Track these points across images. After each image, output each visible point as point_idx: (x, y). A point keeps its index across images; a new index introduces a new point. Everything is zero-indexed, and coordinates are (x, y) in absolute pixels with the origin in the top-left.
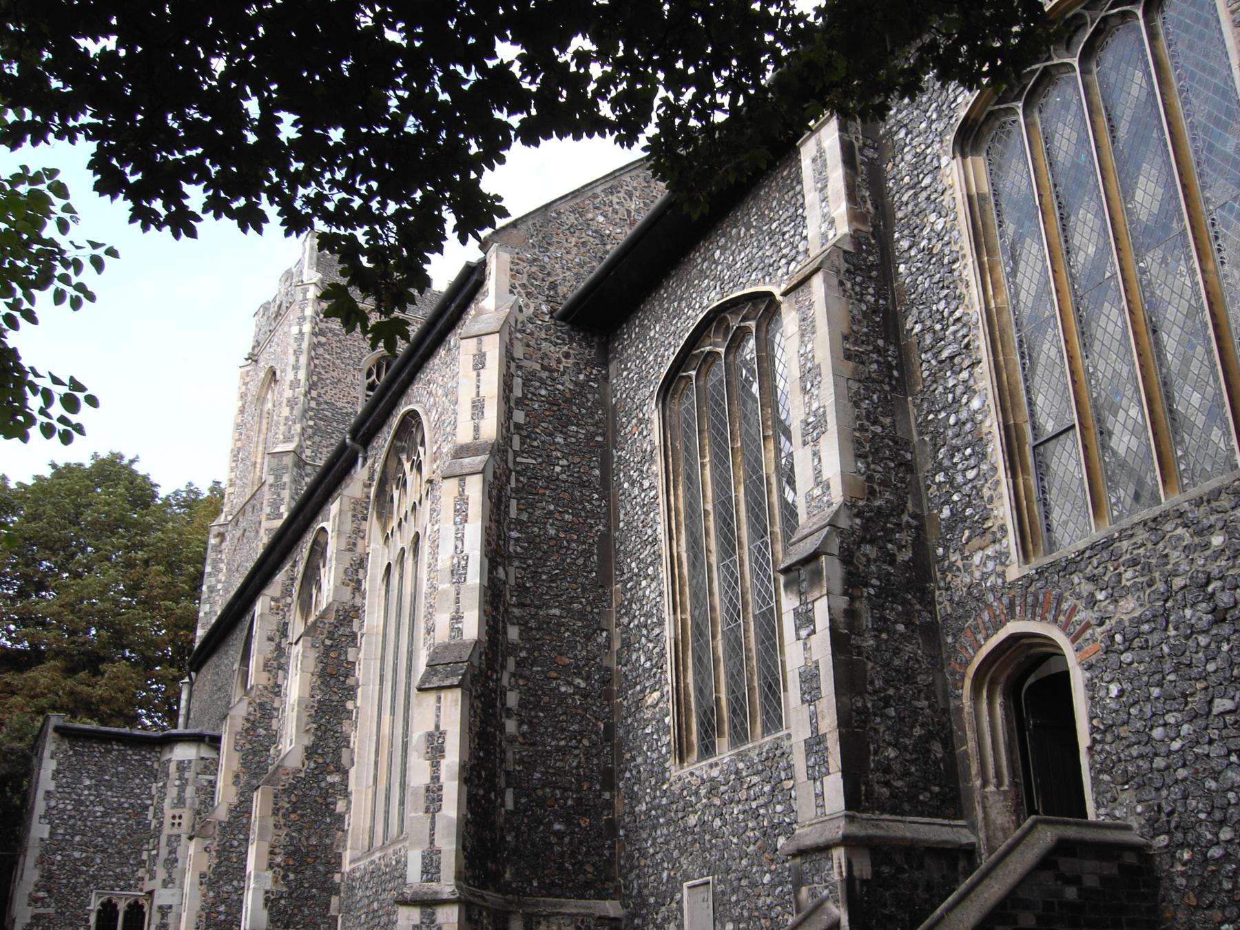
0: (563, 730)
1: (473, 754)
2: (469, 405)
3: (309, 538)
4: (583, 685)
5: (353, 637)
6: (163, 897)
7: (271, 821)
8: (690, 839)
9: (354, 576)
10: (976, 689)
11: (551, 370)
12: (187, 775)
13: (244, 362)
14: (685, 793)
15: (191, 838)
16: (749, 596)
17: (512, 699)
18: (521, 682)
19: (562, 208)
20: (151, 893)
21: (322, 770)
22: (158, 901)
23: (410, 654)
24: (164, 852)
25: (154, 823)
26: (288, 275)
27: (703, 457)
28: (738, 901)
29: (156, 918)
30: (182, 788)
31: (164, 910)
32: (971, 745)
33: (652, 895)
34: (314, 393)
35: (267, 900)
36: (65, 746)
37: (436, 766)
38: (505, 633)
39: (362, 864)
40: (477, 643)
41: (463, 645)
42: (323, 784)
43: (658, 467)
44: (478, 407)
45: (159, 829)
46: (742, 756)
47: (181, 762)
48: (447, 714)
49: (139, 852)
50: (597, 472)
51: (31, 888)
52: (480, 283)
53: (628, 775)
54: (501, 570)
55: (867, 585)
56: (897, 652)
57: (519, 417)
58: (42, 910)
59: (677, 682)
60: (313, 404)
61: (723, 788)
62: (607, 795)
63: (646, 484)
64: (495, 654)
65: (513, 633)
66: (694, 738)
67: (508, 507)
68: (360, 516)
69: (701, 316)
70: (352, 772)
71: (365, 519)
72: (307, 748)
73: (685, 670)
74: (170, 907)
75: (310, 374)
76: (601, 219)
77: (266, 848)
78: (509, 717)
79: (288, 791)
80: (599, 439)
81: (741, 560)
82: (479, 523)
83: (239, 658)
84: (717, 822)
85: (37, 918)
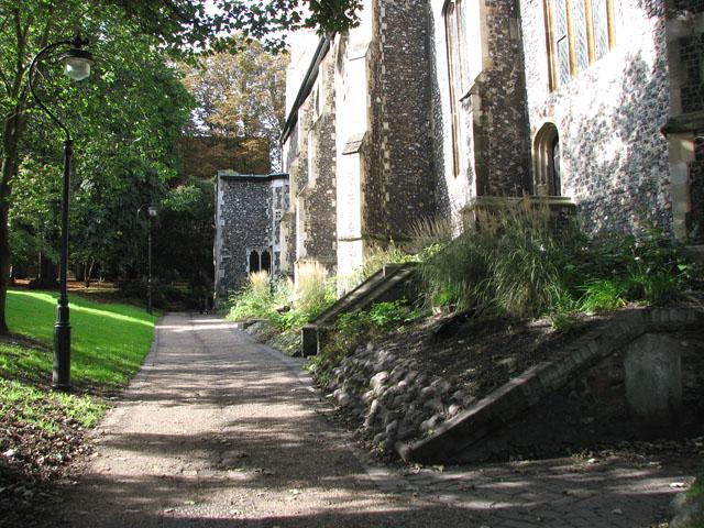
5: (333, 129)
10: (536, 149)
17: (387, 154)
20: (271, 247)
21: (324, 189)
32: (534, 169)
36: (226, 185)
45: (271, 219)
49: (264, 229)
55: (491, 105)
56: (504, 132)
57: (384, 26)
62: (431, 193)
64: (377, 136)
68: (331, 73)
78: (386, 162)
79: (310, 199)
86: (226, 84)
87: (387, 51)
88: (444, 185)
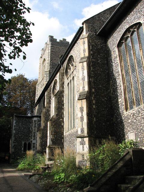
0: (103, 107)
1: (88, 111)
2: (83, 50)
3: (53, 82)
4: (106, 99)
6: (34, 142)
7: (51, 127)
8: (129, 124)
9: (62, 85)
11: (96, 45)
12: (36, 122)
13: (40, 58)
14: (128, 116)
15: (37, 132)
16: (139, 79)
17: (94, 102)
18: (95, 99)
19: (96, 17)
20: (32, 141)
21: (59, 118)
22: (33, 142)
23: (74, 97)
25: (31, 130)
26: (46, 43)
27: (127, 56)
28: (140, 135)
29: (33, 145)
30: (35, 124)
31: (34, 144)
33: (122, 135)
34: (51, 62)
35: (51, 140)
36: (17, 118)
37: (82, 113)
38: (92, 90)
39: (67, 133)
40: (88, 91)
41: (86, 92)
42: (59, 121)
43: (118, 59)
44: (84, 51)
46: (139, 108)
48: (84, 103)
50: (106, 62)
51: (13, 141)
52: (83, 31)
53: (115, 114)
54: (91, 79)
57: (92, 52)
58: (15, 144)
59: (125, 96)
60: (51, 63)
61: (136, 114)
63: (116, 62)
65: (93, 90)
66: (128, 106)
67: (91, 68)
69: (125, 30)
70: (64, 118)
71: (64, 76)
72: (56, 115)
73: (126, 94)
74: (35, 143)
75: (50, 59)
76: (103, 18)
77: (51, 131)
78: (94, 105)
79: (54, 122)
80: (106, 56)
81: (137, 73)
82: (86, 70)
83: (43, 103)
84: (135, 121)
85: (14, 145)
86: (15, 91)
87: (93, 62)
88: (119, 115)
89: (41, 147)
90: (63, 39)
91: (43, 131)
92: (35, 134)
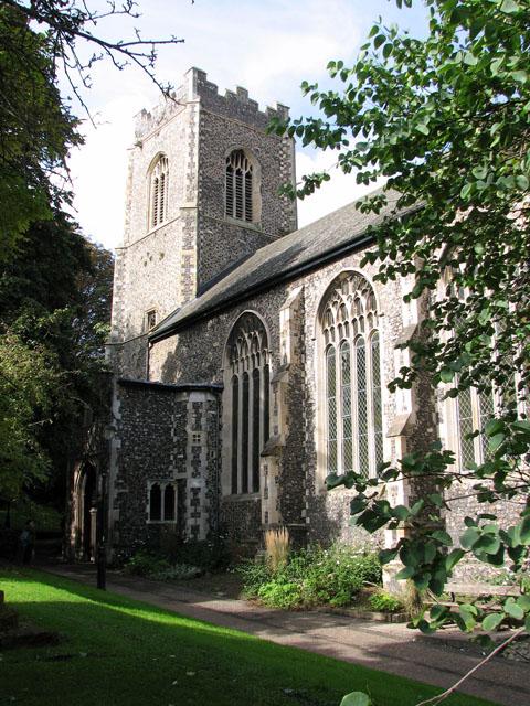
12: (200, 411)
24: (190, 457)
30: (198, 419)
47: (194, 403)
58: (122, 491)
85: (120, 494)
89: (282, 512)
90: (240, 89)
91: (284, 453)
92: (196, 456)
